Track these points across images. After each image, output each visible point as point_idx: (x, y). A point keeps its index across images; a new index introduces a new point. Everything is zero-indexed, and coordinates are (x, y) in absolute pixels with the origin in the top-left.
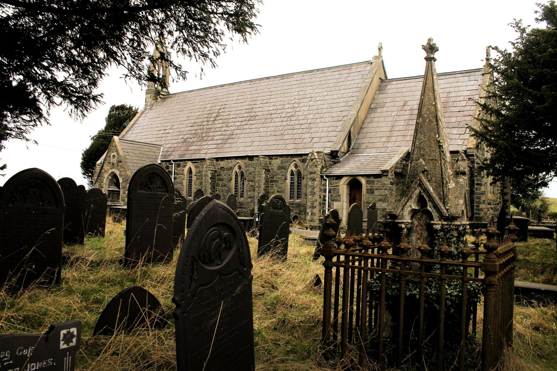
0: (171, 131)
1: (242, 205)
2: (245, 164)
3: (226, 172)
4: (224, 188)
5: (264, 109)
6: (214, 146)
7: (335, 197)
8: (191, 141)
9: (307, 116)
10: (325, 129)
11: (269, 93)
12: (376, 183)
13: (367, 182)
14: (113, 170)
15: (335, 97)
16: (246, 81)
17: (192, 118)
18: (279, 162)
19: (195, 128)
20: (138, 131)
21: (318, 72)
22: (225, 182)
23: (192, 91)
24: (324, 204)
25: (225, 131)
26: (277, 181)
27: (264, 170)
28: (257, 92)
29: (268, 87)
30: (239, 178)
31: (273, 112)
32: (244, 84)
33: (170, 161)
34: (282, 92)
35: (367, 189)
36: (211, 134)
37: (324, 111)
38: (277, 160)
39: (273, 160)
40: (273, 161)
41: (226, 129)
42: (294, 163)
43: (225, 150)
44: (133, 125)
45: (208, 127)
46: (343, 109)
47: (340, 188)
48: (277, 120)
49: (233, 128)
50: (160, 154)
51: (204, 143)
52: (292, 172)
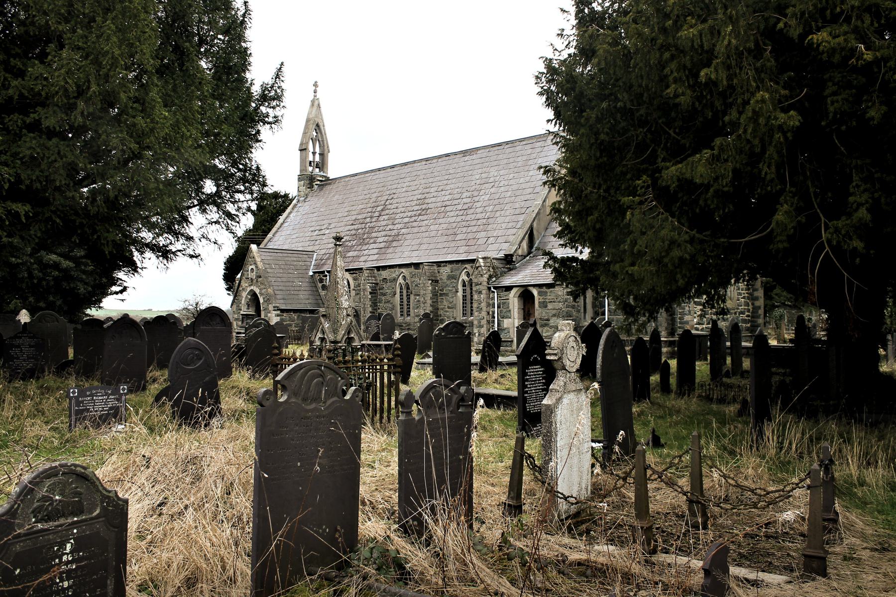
0: (327, 231)
1: (408, 325)
2: (411, 273)
3: (389, 284)
4: (387, 305)
5: (439, 199)
6: (376, 251)
7: (505, 314)
8: (350, 244)
9: (486, 208)
10: (504, 226)
11: (447, 177)
12: (548, 294)
13: (539, 293)
14: (252, 288)
15: (522, 180)
16: (421, 160)
17: (353, 213)
18: (449, 271)
19: (356, 227)
20: (288, 232)
21: (507, 146)
22: (388, 297)
23: (356, 175)
24: (493, 322)
25: (390, 230)
26: (447, 295)
27: (430, 282)
28: (433, 175)
29: (447, 167)
30: (405, 292)
31: (448, 203)
32: (419, 164)
33: (323, 272)
34: (462, 174)
35: (539, 302)
36: (374, 235)
37: (507, 200)
38: (446, 268)
39: (442, 268)
40: (442, 269)
41: (391, 227)
42: (465, 270)
43: (389, 256)
44: (282, 224)
45: (372, 225)
46: (528, 197)
47: (510, 301)
48: (452, 214)
49: (399, 226)
50: (313, 263)
51: (365, 247)
52: (464, 281)
